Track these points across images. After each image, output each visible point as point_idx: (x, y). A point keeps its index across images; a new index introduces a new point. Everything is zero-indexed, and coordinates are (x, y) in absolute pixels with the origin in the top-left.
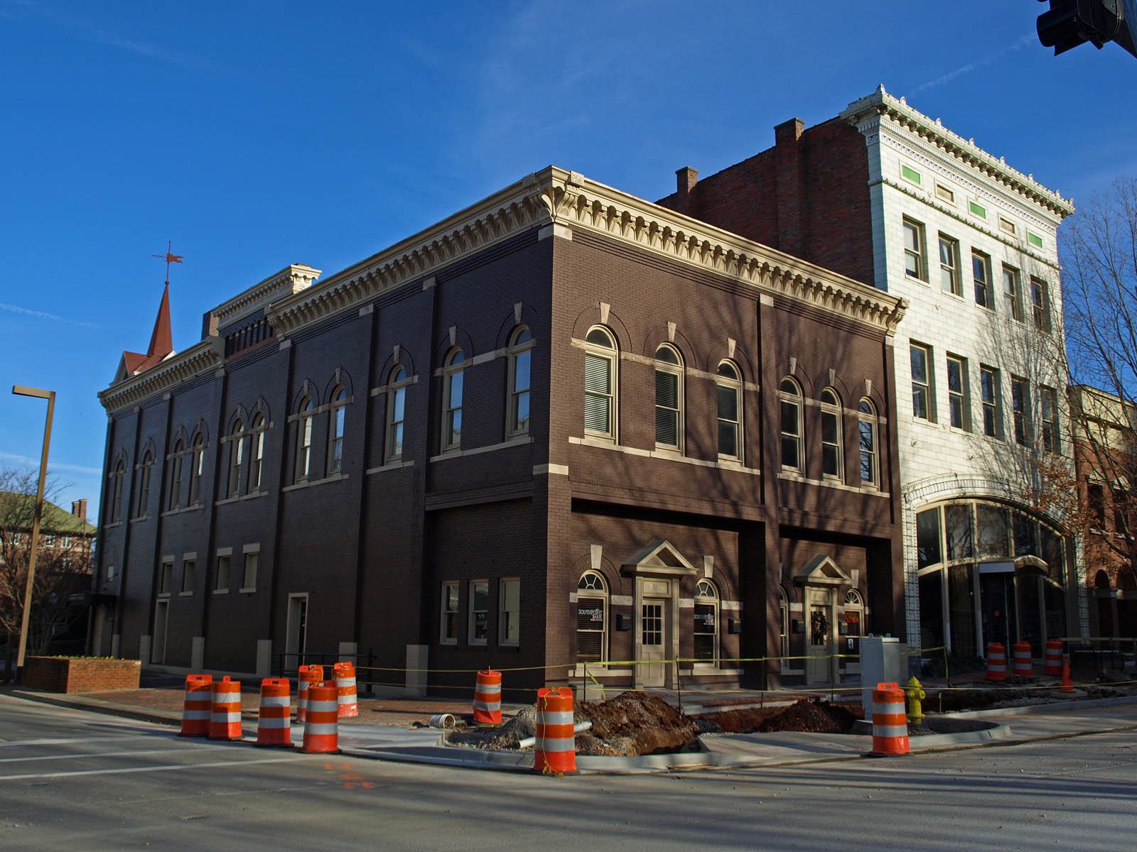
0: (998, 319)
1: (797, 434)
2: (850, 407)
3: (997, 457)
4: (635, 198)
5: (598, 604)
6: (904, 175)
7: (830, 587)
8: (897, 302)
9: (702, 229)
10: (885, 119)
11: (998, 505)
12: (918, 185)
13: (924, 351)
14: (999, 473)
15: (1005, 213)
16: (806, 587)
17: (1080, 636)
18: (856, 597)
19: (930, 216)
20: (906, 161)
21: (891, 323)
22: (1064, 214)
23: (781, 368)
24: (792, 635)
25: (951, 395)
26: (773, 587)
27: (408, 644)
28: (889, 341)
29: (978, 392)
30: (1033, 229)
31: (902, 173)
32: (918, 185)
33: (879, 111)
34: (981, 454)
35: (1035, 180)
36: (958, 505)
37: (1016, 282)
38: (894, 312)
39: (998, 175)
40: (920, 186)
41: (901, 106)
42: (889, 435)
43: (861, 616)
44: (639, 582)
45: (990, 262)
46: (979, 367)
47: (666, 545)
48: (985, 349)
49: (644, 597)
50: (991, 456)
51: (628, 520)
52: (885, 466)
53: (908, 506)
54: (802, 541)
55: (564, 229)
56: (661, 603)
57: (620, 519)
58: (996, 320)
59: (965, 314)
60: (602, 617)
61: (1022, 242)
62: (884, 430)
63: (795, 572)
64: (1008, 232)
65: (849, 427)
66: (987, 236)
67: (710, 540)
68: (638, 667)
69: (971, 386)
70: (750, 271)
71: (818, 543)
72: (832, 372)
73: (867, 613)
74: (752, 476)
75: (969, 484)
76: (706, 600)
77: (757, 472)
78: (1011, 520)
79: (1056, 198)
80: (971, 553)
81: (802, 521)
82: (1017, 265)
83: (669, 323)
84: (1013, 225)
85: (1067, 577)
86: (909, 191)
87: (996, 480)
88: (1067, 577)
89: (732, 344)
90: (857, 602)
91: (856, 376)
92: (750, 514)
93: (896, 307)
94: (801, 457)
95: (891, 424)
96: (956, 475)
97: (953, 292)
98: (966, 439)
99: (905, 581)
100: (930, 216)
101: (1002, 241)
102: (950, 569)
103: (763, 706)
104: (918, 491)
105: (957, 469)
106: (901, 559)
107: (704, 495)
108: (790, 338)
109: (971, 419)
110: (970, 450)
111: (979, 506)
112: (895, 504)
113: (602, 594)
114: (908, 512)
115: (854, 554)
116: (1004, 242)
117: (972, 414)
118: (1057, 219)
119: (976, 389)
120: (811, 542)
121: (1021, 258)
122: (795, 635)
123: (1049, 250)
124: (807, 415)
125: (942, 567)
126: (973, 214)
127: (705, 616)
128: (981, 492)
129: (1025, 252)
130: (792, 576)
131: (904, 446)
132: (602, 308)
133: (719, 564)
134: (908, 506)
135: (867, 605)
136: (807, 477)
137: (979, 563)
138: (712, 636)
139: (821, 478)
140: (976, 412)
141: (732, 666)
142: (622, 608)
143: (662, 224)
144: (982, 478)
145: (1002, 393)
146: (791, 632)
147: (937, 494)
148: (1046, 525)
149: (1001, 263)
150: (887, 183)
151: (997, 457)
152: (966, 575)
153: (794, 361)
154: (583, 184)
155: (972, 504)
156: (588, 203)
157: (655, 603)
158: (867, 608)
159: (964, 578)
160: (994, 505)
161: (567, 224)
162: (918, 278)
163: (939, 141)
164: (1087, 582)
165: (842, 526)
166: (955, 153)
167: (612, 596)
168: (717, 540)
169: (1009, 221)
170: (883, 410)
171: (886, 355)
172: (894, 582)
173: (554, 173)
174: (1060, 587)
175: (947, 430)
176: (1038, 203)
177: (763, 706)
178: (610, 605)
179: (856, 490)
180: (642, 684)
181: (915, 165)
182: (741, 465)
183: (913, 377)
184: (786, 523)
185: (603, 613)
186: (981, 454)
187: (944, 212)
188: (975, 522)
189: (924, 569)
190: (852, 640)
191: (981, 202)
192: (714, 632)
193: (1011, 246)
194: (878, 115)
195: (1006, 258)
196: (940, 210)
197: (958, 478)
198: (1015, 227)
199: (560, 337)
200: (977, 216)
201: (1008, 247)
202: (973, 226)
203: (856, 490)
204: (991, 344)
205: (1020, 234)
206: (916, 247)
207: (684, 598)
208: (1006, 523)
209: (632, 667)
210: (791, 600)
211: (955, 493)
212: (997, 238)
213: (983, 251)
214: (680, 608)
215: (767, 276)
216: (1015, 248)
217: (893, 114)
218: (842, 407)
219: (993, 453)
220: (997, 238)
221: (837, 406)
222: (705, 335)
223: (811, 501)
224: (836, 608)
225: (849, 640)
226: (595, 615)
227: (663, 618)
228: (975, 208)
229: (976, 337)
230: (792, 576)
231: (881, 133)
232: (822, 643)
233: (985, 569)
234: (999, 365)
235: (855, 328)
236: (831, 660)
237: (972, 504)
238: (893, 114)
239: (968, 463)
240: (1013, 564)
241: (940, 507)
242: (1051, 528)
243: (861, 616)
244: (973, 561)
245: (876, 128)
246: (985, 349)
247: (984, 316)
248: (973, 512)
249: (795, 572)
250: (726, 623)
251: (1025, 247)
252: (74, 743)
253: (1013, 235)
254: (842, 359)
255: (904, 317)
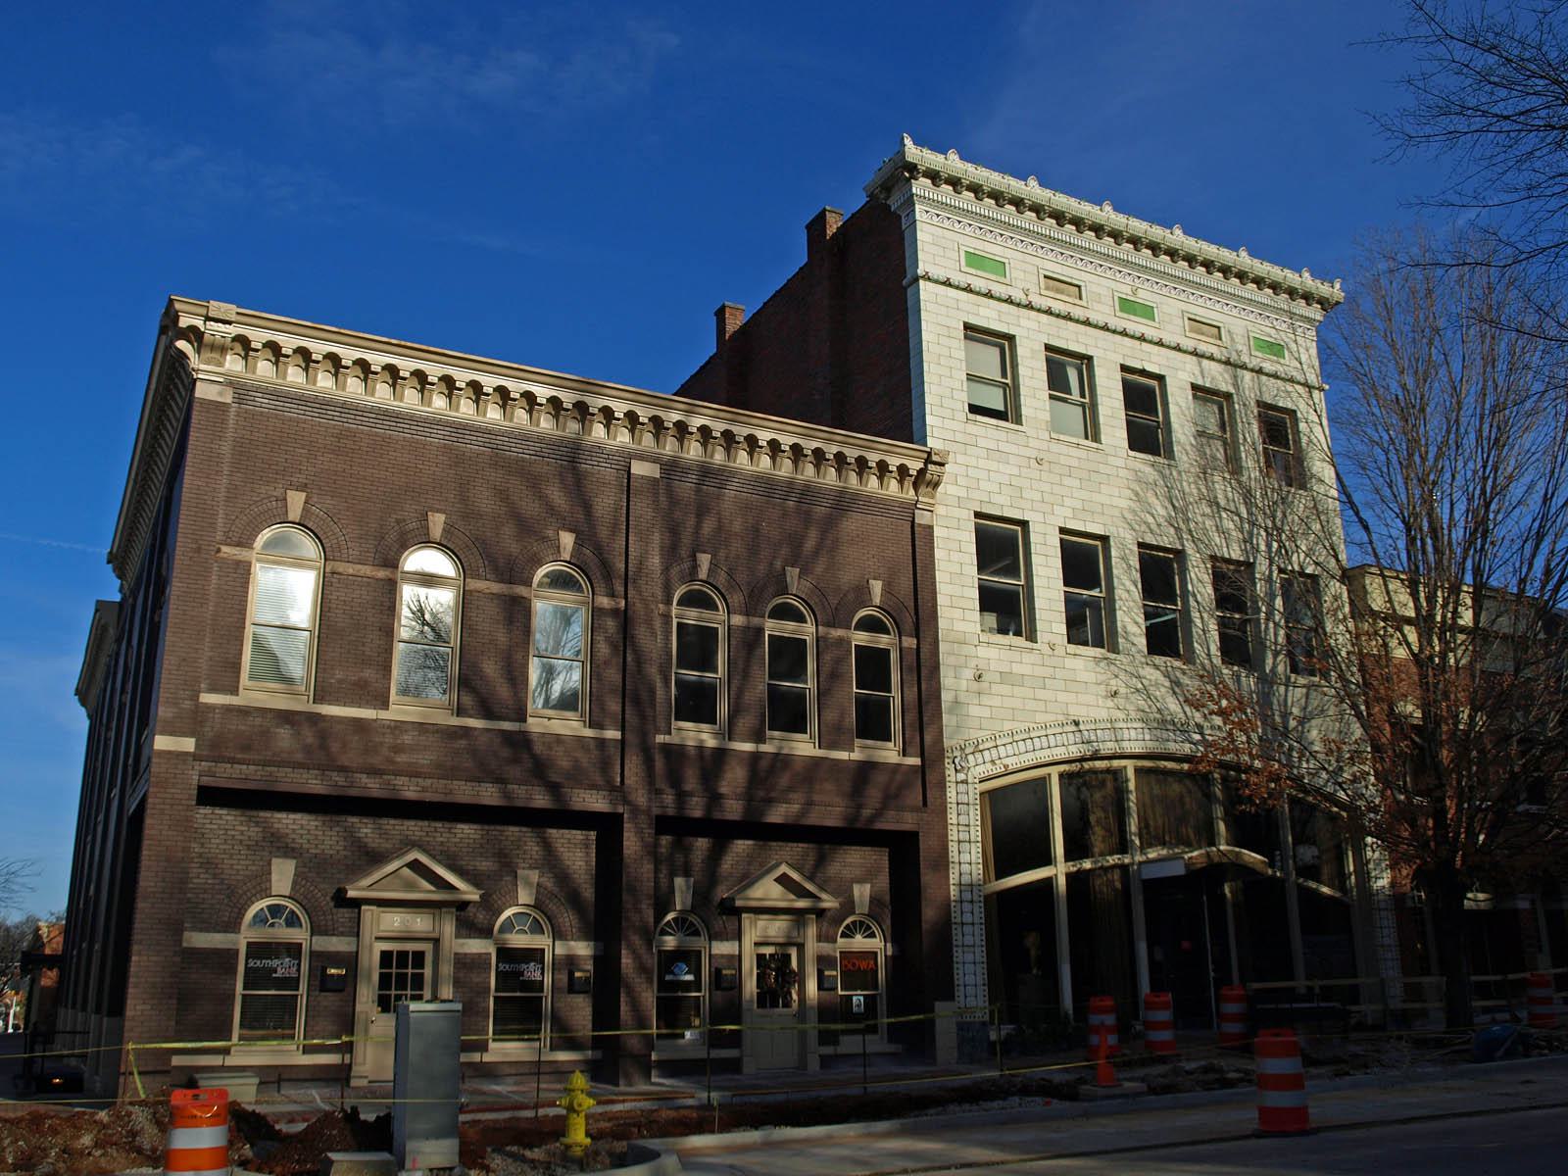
0: (1179, 473)
1: (806, 683)
2: (831, 624)
3: (1177, 690)
4: (342, 331)
5: (294, 950)
6: (1121, 310)
7: (798, 915)
8: (925, 456)
9: (374, 345)
10: (920, 186)
11: (1186, 766)
12: (1002, 280)
13: (1017, 531)
14: (1182, 715)
15: (1050, 266)
16: (744, 915)
17: (1406, 985)
18: (870, 928)
19: (1023, 322)
20: (1125, 291)
21: (922, 489)
22: (1323, 302)
23: (675, 571)
24: (714, 992)
25: (1069, 600)
26: (635, 918)
27: (937, 1000)
28: (922, 518)
29: (1133, 588)
30: (1059, 271)
31: (1117, 308)
32: (1002, 280)
33: (907, 175)
34: (1140, 686)
35: (1251, 254)
36: (1094, 772)
37: (1229, 413)
38: (922, 472)
39: (1242, 276)
40: (1007, 281)
41: (952, 163)
42: (924, 668)
43: (881, 960)
44: (369, 914)
45: (1165, 385)
46: (1136, 549)
47: (784, 869)
48: (1150, 520)
49: (376, 938)
50: (1163, 690)
51: (262, 814)
52: (912, 716)
53: (961, 776)
54: (740, 842)
55: (218, 387)
56: (427, 947)
57: (336, 818)
58: (1175, 473)
59: (1102, 468)
60: (299, 970)
61: (1239, 353)
62: (911, 659)
63: (722, 892)
64: (1212, 341)
65: (827, 657)
66: (1157, 348)
67: (533, 848)
68: (359, 1049)
69: (1115, 580)
70: (681, 440)
71: (845, 847)
72: (793, 573)
73: (889, 953)
74: (602, 743)
75: (1107, 735)
76: (519, 940)
77: (613, 734)
78: (1218, 791)
79: (1305, 280)
80: (1123, 847)
81: (709, 808)
82: (1225, 386)
83: (698, 555)
84: (1079, 287)
85: (1353, 877)
86: (1111, 326)
87: (1171, 727)
88: (1353, 877)
89: (567, 540)
90: (872, 935)
91: (847, 577)
92: (595, 802)
93: (926, 464)
94: (723, 709)
95: (925, 649)
96: (1077, 723)
97: (1087, 438)
98: (1102, 664)
99: (952, 898)
100: (1064, 334)
101: (1191, 353)
102: (1069, 876)
103: (539, 1114)
104: (986, 753)
105: (1077, 712)
106: (942, 862)
107: (485, 773)
108: (698, 526)
109: (1117, 632)
110: (1113, 682)
111: (1138, 771)
112: (931, 777)
113: (300, 935)
114: (962, 788)
115: (853, 860)
116: (1195, 353)
117: (1119, 624)
118: (1315, 313)
119: (1128, 584)
120: (761, 843)
121: (1235, 377)
122: (719, 992)
123: (1303, 357)
124: (733, 642)
125: (1054, 872)
126: (1125, 316)
127: (524, 966)
128: (1136, 748)
129: (1244, 367)
130: (717, 899)
131: (953, 682)
132: (289, 499)
133: (549, 883)
134: (961, 776)
135: (889, 938)
136: (904, 755)
137: (1140, 863)
138: (541, 998)
139: (759, 737)
140: (1127, 619)
141: (572, 1044)
142: (335, 959)
143: (809, 445)
144: (1139, 725)
145: (1190, 587)
146: (713, 987)
147: (1030, 756)
148: (1301, 795)
149: (1189, 387)
150: (929, 279)
151: (1177, 690)
152: (1118, 885)
153: (704, 560)
154: (234, 318)
155: (1125, 767)
156: (805, 451)
157: (410, 947)
158: (889, 945)
159: (1115, 889)
160: (1179, 767)
161: (221, 380)
162: (1007, 420)
163: (1038, 209)
164: (1393, 884)
165: (803, 813)
166: (1096, 232)
167: (314, 938)
168: (547, 846)
169: (1069, 280)
170: (908, 622)
171: (919, 543)
172: (923, 903)
173: (177, 306)
174: (1338, 895)
175: (1060, 651)
176: (1269, 291)
177: (539, 1114)
178: (311, 952)
179: (843, 755)
180: (366, 1077)
181: (994, 249)
182: (585, 726)
183: (1066, 584)
184: (671, 812)
185: (299, 965)
186: (1140, 686)
187: (1058, 316)
188: (1133, 797)
189: (1003, 880)
190: (862, 998)
191: (1144, 296)
192: (542, 991)
193: (1211, 358)
194: (908, 180)
195: (1200, 377)
196: (1049, 312)
197: (1082, 727)
198: (1222, 330)
199: (194, 546)
200: (1132, 317)
201: (1205, 362)
202: (1124, 333)
203: (843, 755)
204: (1162, 512)
205: (1232, 340)
206: (1004, 375)
207: (470, 938)
208: (1209, 796)
209: (349, 1048)
210: (715, 936)
211: (1075, 751)
212: (1177, 348)
213: (1147, 369)
214: (456, 954)
215: (908, 483)
216: (1219, 361)
217: (934, 176)
218: (817, 625)
219: (1167, 684)
220: (1177, 348)
221: (809, 625)
222: (508, 530)
223: (733, 779)
224: (813, 947)
225: (854, 998)
226: (282, 967)
227: (428, 971)
228: (1127, 306)
229: (1131, 503)
230: (717, 899)
231: (918, 207)
232: (787, 1005)
233: (1149, 873)
234: (1180, 538)
235: (844, 502)
236: (803, 1035)
237: (1125, 767)
238: (934, 176)
239: (1110, 703)
240: (1181, 861)
241: (1049, 775)
242: (1336, 809)
243: (881, 960)
244: (1127, 861)
245: (909, 202)
246: (1150, 520)
247: (1148, 470)
248: (1127, 780)
249: (722, 892)
250: (564, 977)
251: (1245, 359)
252: (510, 1119)
253: (1219, 342)
254: (817, 552)
255: (945, 479)
